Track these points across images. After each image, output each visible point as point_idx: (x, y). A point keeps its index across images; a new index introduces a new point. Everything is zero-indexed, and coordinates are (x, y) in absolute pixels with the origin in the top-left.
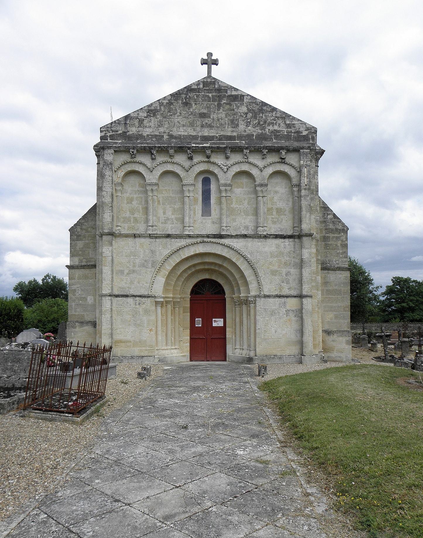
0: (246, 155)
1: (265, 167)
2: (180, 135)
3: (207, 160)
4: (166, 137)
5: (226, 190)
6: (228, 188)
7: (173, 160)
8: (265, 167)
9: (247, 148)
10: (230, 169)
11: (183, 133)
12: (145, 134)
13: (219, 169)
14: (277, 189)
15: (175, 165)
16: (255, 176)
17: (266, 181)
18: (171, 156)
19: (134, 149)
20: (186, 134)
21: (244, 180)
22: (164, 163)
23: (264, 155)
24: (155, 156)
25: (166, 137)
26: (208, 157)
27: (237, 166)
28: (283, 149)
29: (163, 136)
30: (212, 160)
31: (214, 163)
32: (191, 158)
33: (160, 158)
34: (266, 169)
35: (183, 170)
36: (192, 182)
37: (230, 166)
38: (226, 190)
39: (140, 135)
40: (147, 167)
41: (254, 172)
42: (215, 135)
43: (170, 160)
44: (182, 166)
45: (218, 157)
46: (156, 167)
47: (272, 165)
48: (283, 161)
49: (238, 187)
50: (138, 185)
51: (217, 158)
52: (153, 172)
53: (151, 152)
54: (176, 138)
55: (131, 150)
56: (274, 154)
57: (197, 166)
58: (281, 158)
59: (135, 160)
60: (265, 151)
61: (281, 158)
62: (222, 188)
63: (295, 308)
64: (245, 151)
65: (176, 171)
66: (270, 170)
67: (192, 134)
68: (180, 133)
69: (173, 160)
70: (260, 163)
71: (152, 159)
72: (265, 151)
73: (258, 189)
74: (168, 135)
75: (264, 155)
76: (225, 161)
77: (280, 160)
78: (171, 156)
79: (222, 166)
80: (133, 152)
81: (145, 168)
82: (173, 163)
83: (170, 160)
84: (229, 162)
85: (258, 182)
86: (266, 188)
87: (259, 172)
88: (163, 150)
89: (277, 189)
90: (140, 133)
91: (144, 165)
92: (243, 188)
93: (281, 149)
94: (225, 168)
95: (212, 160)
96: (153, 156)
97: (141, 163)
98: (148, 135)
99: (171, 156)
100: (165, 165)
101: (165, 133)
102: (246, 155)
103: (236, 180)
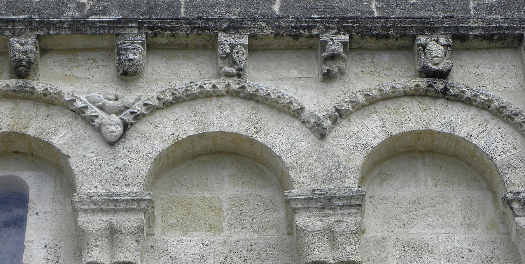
0: (228, 58)
1: (339, 115)
3: (13, 83)
5: (113, 233)
6: (129, 221)
8: (339, 115)
9: (234, 28)
10: (141, 127)
13: (80, 129)
14: (421, 230)
16: (288, 160)
17: (351, 184)
21: (226, 190)
23: (333, 57)
26: (22, 70)
27: (180, 112)
28: (433, 30)
30: (38, 84)
31: (50, 101)
33: (165, 76)
34: (344, 128)
37: (139, 108)
38: (113, 233)
41: (282, 138)
45: (79, 72)
47: (381, 107)
48: (436, 85)
49: (186, 229)
51: (72, 79)
56: (385, 58)
58: (427, 73)
60: (336, 41)
61: (427, 73)
62: (93, 222)
63: (316, 67)
64: (222, 38)
66: (372, 130)
70: (317, 100)
72: (336, 41)
73: (306, 220)
75: (333, 57)
76: (113, 90)
77: (423, 82)
79: (92, 110)
84: (135, 97)
85: (302, 185)
86: (351, 221)
87: (305, 141)
89: (421, 230)
92: (215, 229)
93: (421, 31)
94: (113, 125)
95: (38, 84)
102: (228, 58)
103: (180, 192)
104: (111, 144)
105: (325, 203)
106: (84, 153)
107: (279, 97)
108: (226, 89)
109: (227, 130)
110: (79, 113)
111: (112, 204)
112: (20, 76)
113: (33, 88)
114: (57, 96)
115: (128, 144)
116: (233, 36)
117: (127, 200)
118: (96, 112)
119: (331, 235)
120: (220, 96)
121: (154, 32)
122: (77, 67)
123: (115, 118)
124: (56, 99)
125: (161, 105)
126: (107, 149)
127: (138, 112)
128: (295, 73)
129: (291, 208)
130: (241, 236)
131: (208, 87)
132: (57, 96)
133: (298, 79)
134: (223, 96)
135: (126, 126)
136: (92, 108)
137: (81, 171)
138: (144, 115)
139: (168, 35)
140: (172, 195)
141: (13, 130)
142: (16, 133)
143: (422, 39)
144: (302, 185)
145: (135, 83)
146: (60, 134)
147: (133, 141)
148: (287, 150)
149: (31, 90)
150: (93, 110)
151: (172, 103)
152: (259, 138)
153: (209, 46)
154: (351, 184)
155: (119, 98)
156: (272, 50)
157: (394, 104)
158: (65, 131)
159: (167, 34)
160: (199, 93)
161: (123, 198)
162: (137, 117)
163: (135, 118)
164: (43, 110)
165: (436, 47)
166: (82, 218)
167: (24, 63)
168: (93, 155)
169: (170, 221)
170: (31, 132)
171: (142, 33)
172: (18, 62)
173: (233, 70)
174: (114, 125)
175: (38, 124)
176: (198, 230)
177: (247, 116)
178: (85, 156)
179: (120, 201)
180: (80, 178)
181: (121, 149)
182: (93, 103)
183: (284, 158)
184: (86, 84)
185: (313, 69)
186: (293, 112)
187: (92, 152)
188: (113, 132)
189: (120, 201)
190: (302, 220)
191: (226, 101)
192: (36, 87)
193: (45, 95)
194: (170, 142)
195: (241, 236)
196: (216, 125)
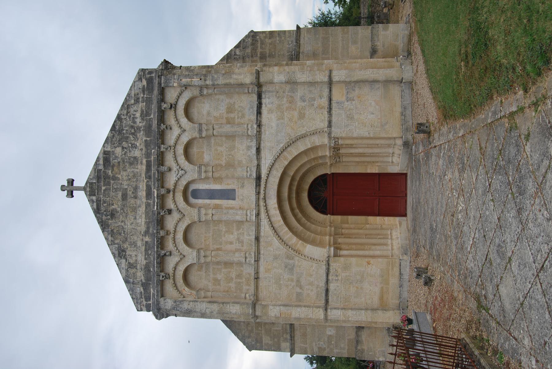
0: (167, 149)
2: (146, 222)
3: (171, 193)
4: (147, 239)
7: (172, 231)
11: (144, 220)
12: (144, 262)
13: (182, 179)
15: (178, 229)
16: (190, 138)
17: (196, 125)
18: (167, 234)
19: (159, 276)
20: (144, 216)
21: (193, 236)
22: (175, 242)
24: (167, 252)
25: (147, 239)
26: (168, 191)
28: (161, 106)
29: (146, 242)
30: (172, 187)
31: (176, 185)
32: (170, 212)
33: (170, 245)
34: (183, 125)
35: (182, 220)
36: (196, 210)
37: (178, 167)
39: (145, 268)
40: (179, 261)
41: (185, 139)
42: (145, 183)
43: (172, 235)
44: (178, 222)
45: (168, 180)
46: (179, 251)
47: (178, 118)
48: (173, 107)
50: (199, 273)
52: (185, 254)
53: (163, 256)
54: (148, 228)
55: (161, 278)
57: (178, 204)
59: (171, 275)
65: (184, 228)
66: (184, 121)
67: (144, 209)
68: (143, 223)
69: (172, 231)
70: (176, 131)
71: (170, 255)
72: (162, 233)
73: (204, 135)
74: (145, 236)
77: (173, 109)
78: (168, 233)
79: (178, 176)
80: (163, 277)
81: (180, 264)
82: (175, 231)
83: (172, 235)
84: (175, 252)
87: (186, 134)
88: (161, 243)
90: (143, 267)
91: (177, 264)
93: (161, 108)
94: (181, 172)
96: (167, 254)
97: (175, 268)
98: (146, 259)
99: (168, 233)
100: (177, 241)
101: (142, 240)
102: (167, 149)
104: (184, 256)
105: (200, 131)
111: (200, 172)
112: (170, 191)
119: (207, 130)
123: (180, 172)
128: (169, 135)
129: (201, 137)
143: (163, 108)
144: (196, 176)
147: (185, 168)
152: (185, 143)
153: (162, 153)
154: (196, 125)
157: (177, 115)
164: (177, 187)
165: (164, 106)
166: (202, 178)
170: (183, 189)
173: (169, 148)
175: (181, 187)
180: (193, 178)
184: (171, 263)
185: (168, 132)
186: (179, 136)
190: (204, 135)
191: (176, 150)
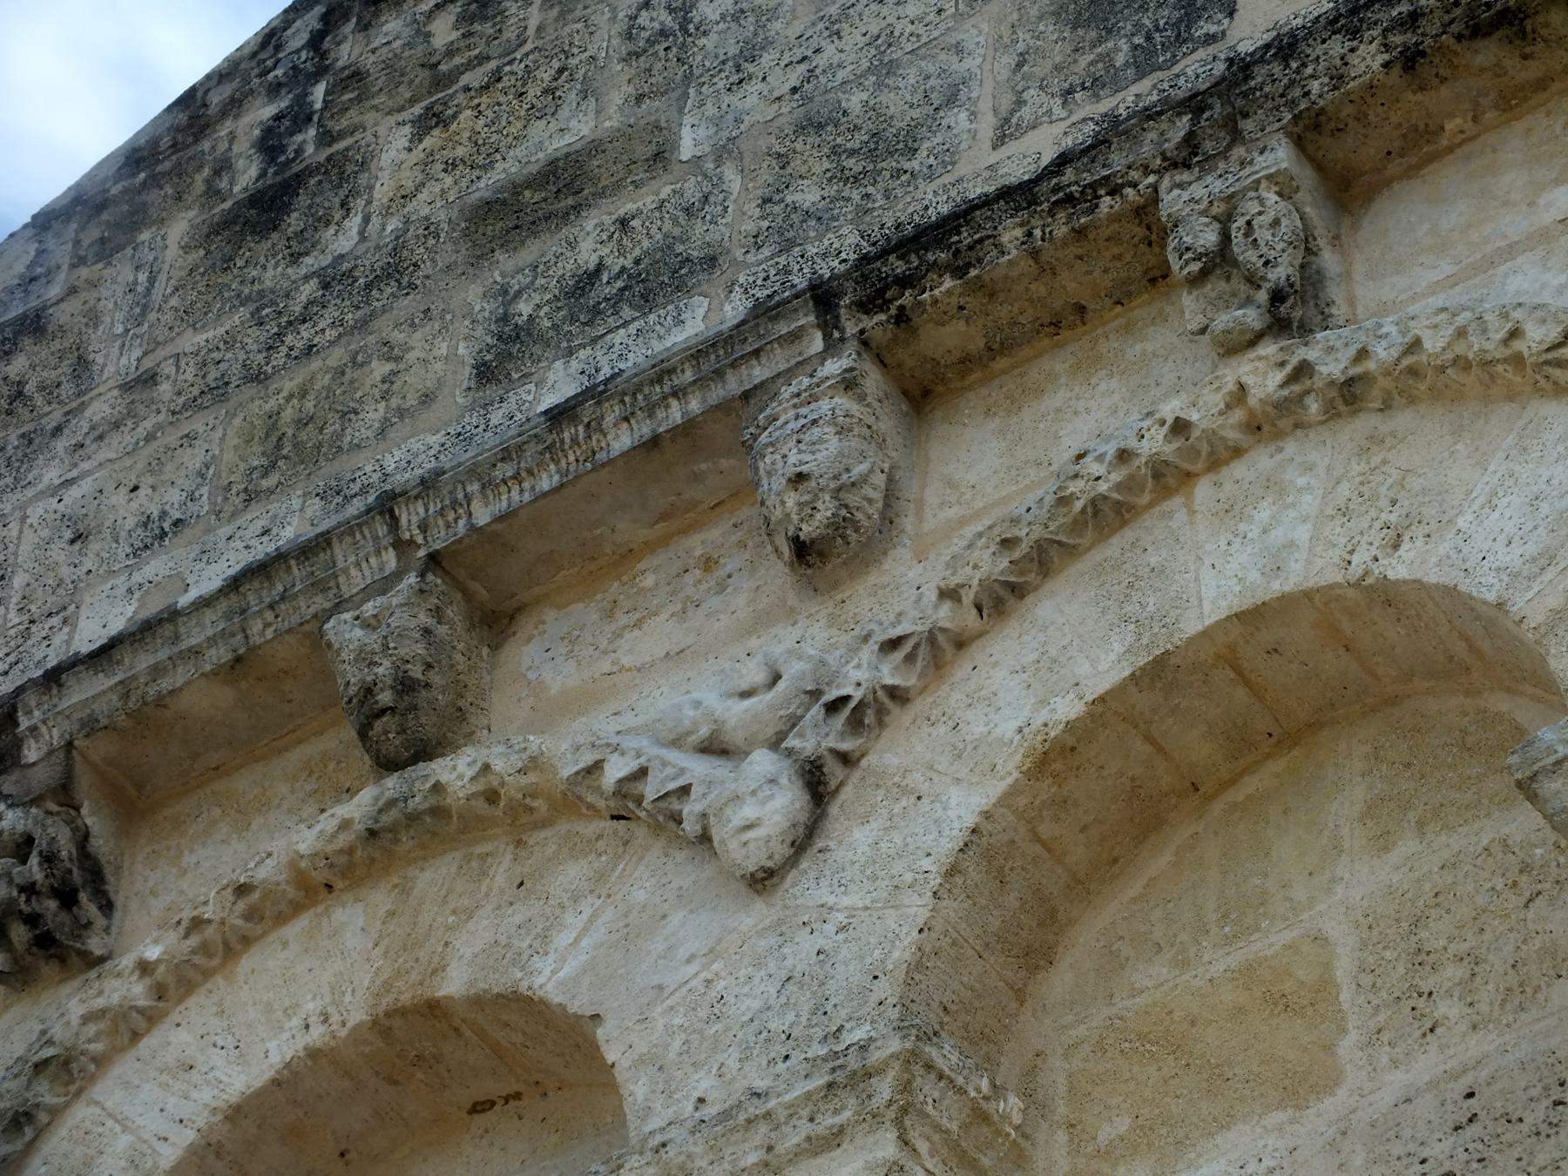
21: (1340, 880)
37: (859, 675)
51: (772, 707)
92: (1300, 1086)
94: (761, 803)
106: (656, 980)
107: (1461, 333)
108: (1238, 415)
109: (1262, 596)
110: (625, 806)
113: (438, 788)
114: (532, 778)
115: (839, 854)
116: (1222, 165)
117: (808, 1096)
118: (682, 771)
120: (1221, 456)
121: (893, 311)
122: (638, 624)
124: (534, 796)
125: (971, 619)
126: (757, 914)
127: (858, 695)
130: (1427, 1064)
131: (1155, 443)
132: (532, 778)
133: (735, 88)
134: (1237, 452)
135: (817, 783)
136: (665, 764)
137: (642, 1061)
138: (896, 695)
139: (954, 300)
140: (1113, 1011)
141: (386, 1002)
142: (402, 1012)
145: (873, 578)
146: (562, 939)
148: (1534, 560)
149: (432, 801)
150: (669, 771)
151: (1017, 591)
153: (1146, 268)
155: (782, 669)
156: (1450, 150)
158: (587, 912)
159: (949, 292)
160: (1118, 487)
161: (787, 1098)
162: (863, 715)
163: (856, 724)
167: (385, 698)
168: (692, 969)
169: (1106, 1133)
170: (454, 984)
171: (842, 340)
172: (361, 703)
174: (754, 793)
176: (1224, 1123)
177: (1344, 490)
178: (660, 988)
179: (782, 1115)
181: (808, 888)
182: (676, 743)
183: (1519, 603)
187: (691, 959)
188: (749, 827)
189: (782, 1115)
192: (444, 778)
193: (492, 796)
194: (1010, 767)
195: (1427, 1064)
196: (1209, 593)
